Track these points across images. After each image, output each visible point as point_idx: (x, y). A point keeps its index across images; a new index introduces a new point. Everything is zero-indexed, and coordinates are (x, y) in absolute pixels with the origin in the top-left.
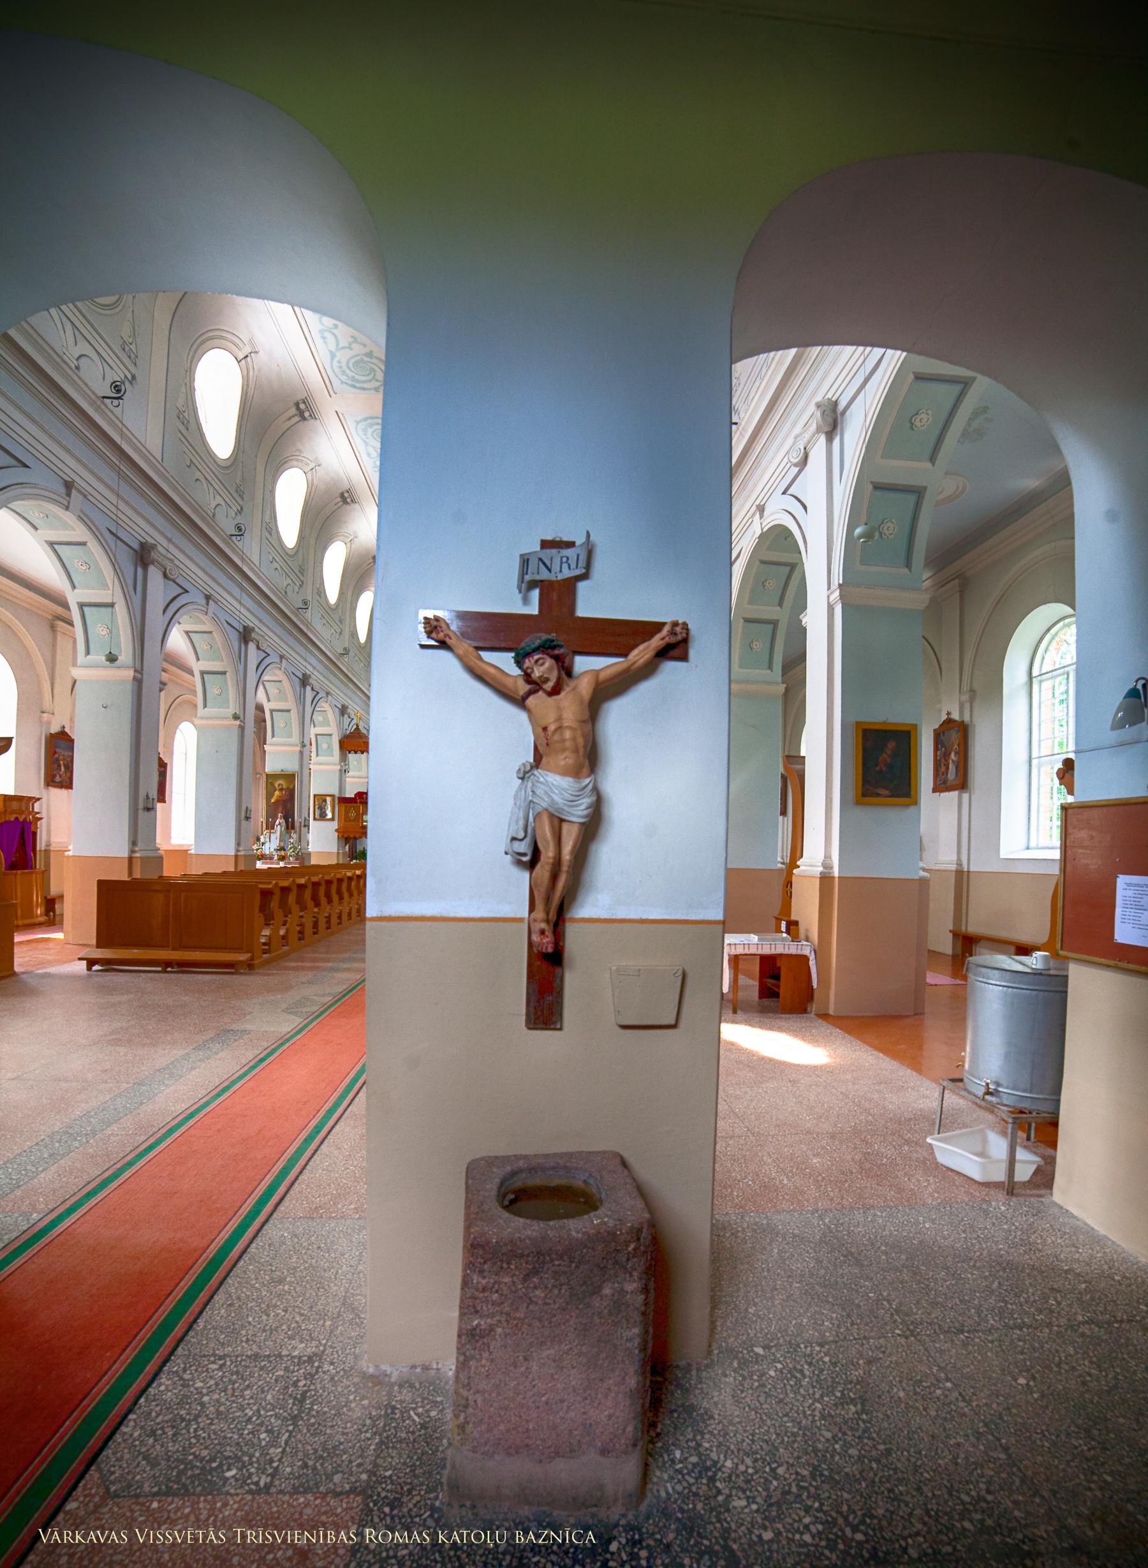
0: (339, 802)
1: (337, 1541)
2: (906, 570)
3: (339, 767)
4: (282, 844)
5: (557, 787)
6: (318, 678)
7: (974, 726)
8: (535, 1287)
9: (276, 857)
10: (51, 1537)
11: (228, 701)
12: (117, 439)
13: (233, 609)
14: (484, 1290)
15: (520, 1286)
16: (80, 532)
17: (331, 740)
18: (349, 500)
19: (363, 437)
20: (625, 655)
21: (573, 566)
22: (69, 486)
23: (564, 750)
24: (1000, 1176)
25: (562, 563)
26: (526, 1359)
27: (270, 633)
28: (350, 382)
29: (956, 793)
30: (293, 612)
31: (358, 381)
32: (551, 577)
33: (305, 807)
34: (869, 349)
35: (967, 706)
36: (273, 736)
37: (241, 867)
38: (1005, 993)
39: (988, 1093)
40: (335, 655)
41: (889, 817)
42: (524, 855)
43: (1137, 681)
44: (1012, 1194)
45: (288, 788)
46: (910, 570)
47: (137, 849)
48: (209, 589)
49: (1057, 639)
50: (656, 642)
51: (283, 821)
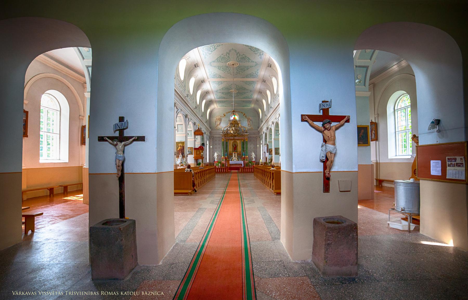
1: (144, 294)
2: (364, 87)
3: (194, 140)
5: (331, 147)
6: (190, 116)
7: (379, 123)
8: (339, 235)
9: (180, 165)
10: (292, 260)
14: (330, 236)
15: (336, 235)
18: (197, 66)
19: (203, 50)
20: (340, 122)
21: (329, 106)
23: (332, 140)
24: (407, 229)
25: (326, 105)
26: (338, 248)
29: (375, 141)
30: (184, 98)
32: (325, 108)
33: (186, 152)
35: (377, 118)
38: (405, 188)
39: (402, 210)
40: (193, 108)
41: (363, 148)
42: (324, 160)
43: (433, 120)
44: (410, 232)
45: (182, 146)
46: (365, 86)
49: (402, 99)
50: (345, 120)
51: (181, 155)
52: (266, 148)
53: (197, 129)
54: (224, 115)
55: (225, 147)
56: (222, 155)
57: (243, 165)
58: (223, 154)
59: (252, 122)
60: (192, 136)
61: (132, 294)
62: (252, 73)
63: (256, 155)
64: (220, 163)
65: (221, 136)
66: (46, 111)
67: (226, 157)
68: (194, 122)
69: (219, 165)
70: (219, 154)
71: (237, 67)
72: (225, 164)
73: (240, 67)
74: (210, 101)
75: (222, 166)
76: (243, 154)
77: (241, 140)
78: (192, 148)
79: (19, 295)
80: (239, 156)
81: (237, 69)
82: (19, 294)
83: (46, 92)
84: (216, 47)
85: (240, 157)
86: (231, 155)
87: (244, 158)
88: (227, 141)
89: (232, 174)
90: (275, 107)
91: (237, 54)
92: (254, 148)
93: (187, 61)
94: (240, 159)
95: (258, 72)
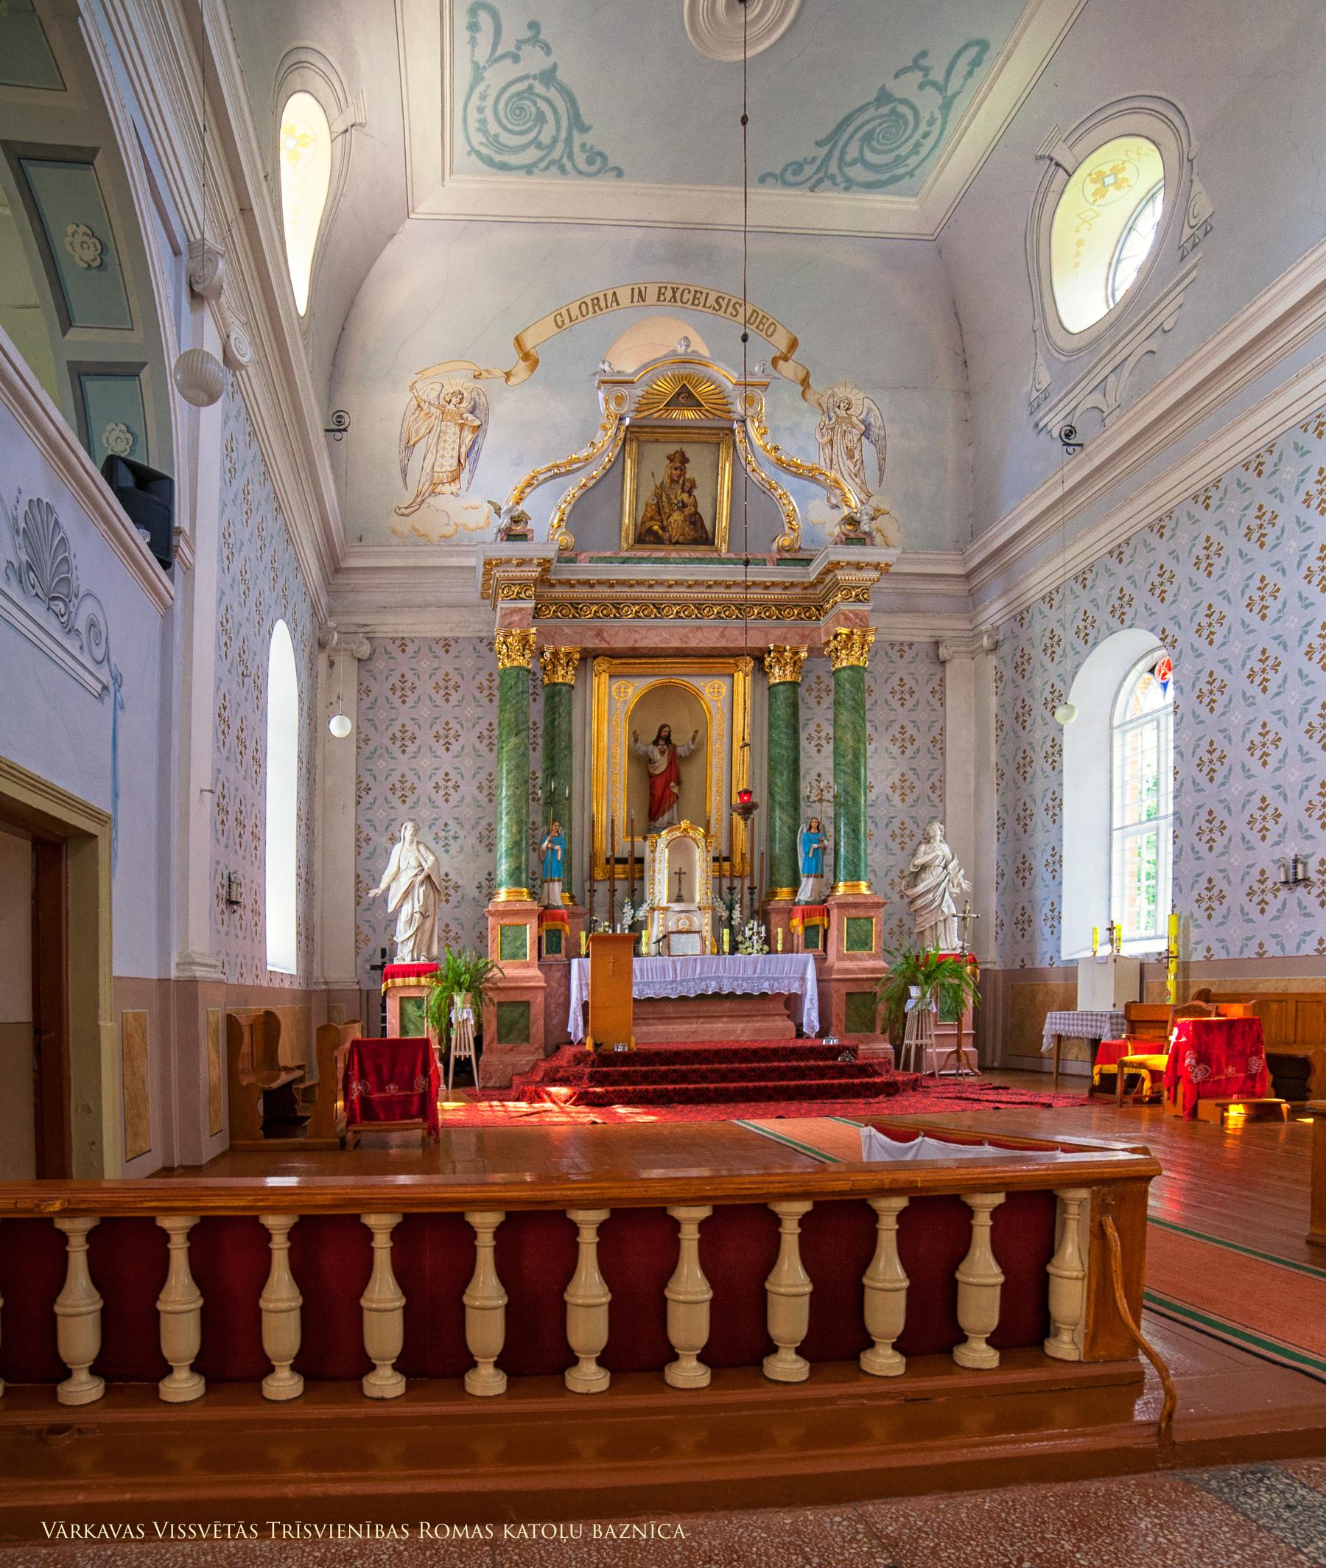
1: (604, 1535)
28: (484, 151)
31: (496, 143)
34: (1112, 306)
54: (526, 356)
56: (504, 867)
59: (881, 452)
61: (549, 1532)
64: (476, 985)
67: (557, 894)
72: (538, 1001)
75: (502, 1035)
77: (761, 669)
79: (70, 1539)
82: (69, 1534)
86: (611, 878)
87: (821, 906)
88: (563, 675)
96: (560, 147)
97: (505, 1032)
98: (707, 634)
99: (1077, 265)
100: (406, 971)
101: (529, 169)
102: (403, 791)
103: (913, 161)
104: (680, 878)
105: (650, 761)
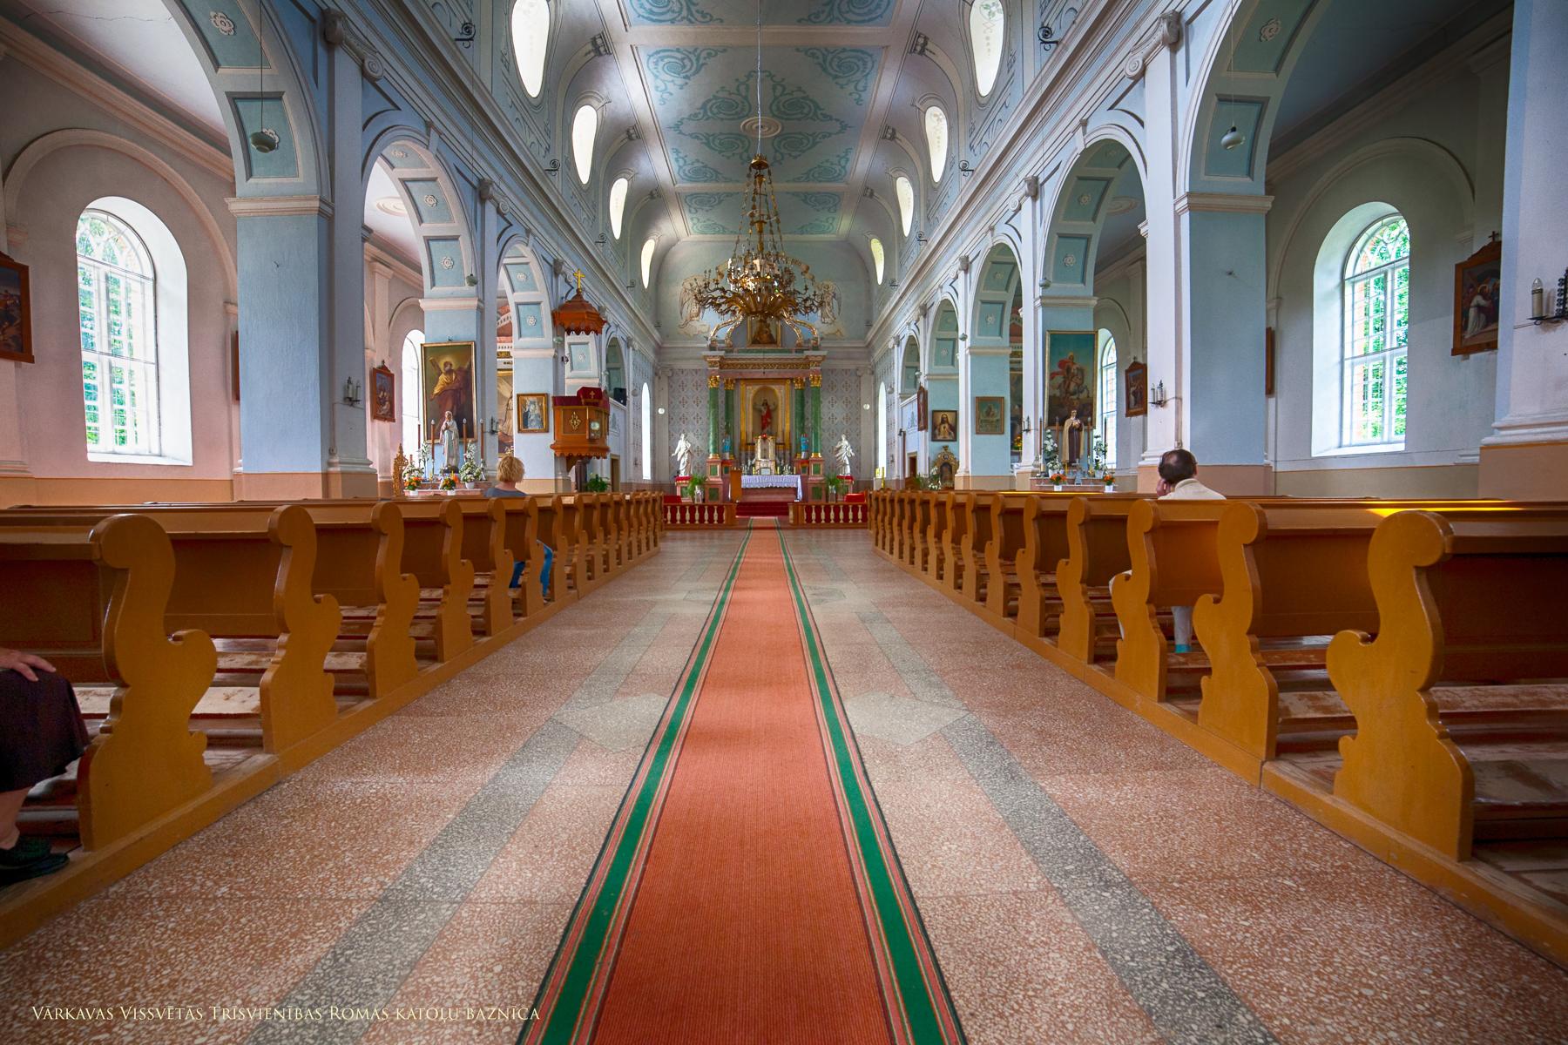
0: (555, 404)
4: (453, 462)
11: (295, 162)
12: (467, 83)
13: (464, 152)
16: (434, 169)
17: (540, 309)
19: (655, 71)
22: (429, 125)
27: (508, 192)
28: (646, 15)
36: (433, 285)
37: (337, 494)
45: (460, 369)
47: (336, 460)
48: (429, 114)
51: (453, 424)
52: (914, 408)
53: (569, 298)
55: (722, 414)
56: (711, 448)
57: (800, 494)
58: (715, 442)
60: (542, 336)
62: (827, 161)
63: (857, 448)
64: (702, 483)
65: (705, 365)
66: (103, 279)
67: (727, 456)
68: (556, 261)
69: (698, 491)
70: (698, 443)
71: (776, 137)
73: (785, 139)
74: (652, 195)
76: (798, 445)
77: (792, 384)
78: (545, 395)
80: (784, 454)
81: (775, 144)
83: (90, 206)
84: (701, 61)
85: (788, 456)
86: (747, 450)
87: (807, 461)
88: (731, 387)
89: (754, 534)
90: (924, 254)
91: (774, 89)
92: (847, 419)
93: (600, 111)
94: (787, 468)
95: (848, 160)
96: (685, 13)
97: (711, 497)
98: (774, 373)
99: (989, 50)
100: (682, 479)
101: (673, 21)
102: (684, 419)
103: (879, 12)
104: (765, 451)
105: (761, 411)
